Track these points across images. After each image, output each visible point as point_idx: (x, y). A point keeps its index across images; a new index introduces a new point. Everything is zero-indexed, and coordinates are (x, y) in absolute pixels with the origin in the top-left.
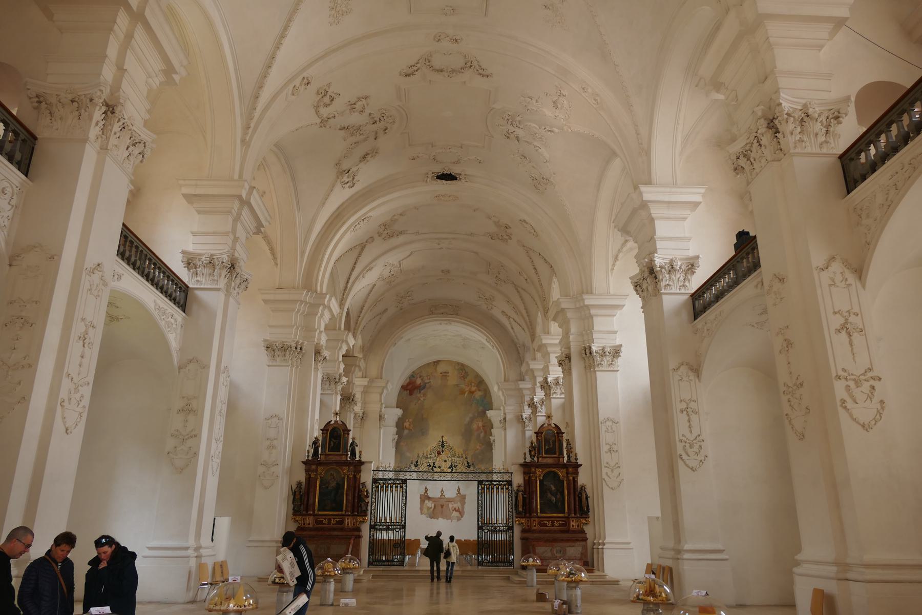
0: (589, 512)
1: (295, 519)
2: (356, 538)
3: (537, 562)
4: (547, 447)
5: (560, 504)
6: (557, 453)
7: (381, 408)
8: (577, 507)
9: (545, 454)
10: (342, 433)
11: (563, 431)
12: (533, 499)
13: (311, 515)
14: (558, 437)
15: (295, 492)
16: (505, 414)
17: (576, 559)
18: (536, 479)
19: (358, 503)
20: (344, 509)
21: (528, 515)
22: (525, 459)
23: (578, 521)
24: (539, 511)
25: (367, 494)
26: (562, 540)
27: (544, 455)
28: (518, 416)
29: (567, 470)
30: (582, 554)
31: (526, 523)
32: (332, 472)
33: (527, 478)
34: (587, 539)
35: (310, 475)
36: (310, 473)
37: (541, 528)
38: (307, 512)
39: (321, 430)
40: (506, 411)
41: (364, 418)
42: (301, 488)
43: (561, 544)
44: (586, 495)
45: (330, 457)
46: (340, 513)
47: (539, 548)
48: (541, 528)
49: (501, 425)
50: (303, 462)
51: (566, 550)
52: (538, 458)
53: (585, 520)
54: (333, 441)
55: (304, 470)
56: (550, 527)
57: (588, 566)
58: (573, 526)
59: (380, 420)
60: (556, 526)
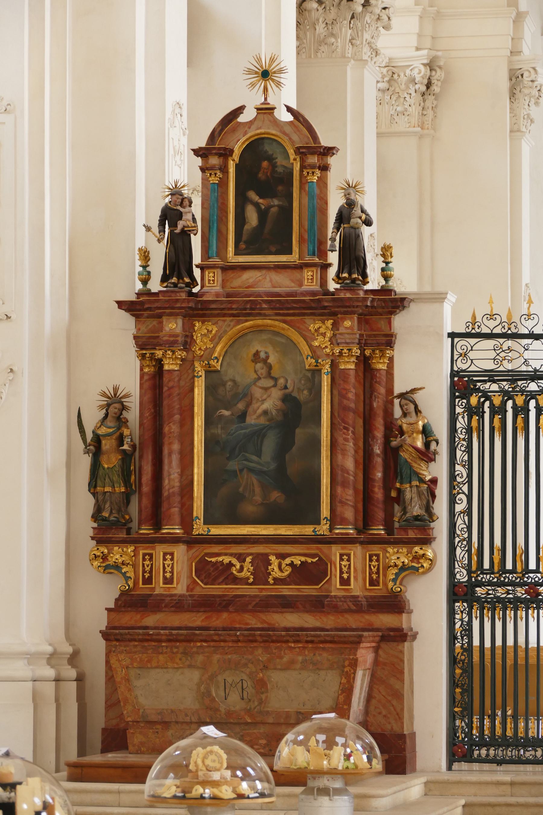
1: (105, 558)
2: (384, 639)
7: (516, 39)
10: (297, 167)
13: (175, 540)
15: (97, 440)
19: (387, 485)
20: (325, 511)
25: (427, 445)
32: (257, 346)
35: (159, 363)
36: (159, 354)
38: (157, 525)
39: (197, 152)
41: (436, 88)
42: (121, 422)
45: (249, 277)
46: (308, 530)
50: (121, 304)
54: (257, 205)
55: (132, 342)
59: (512, 95)
60: (277, 581)
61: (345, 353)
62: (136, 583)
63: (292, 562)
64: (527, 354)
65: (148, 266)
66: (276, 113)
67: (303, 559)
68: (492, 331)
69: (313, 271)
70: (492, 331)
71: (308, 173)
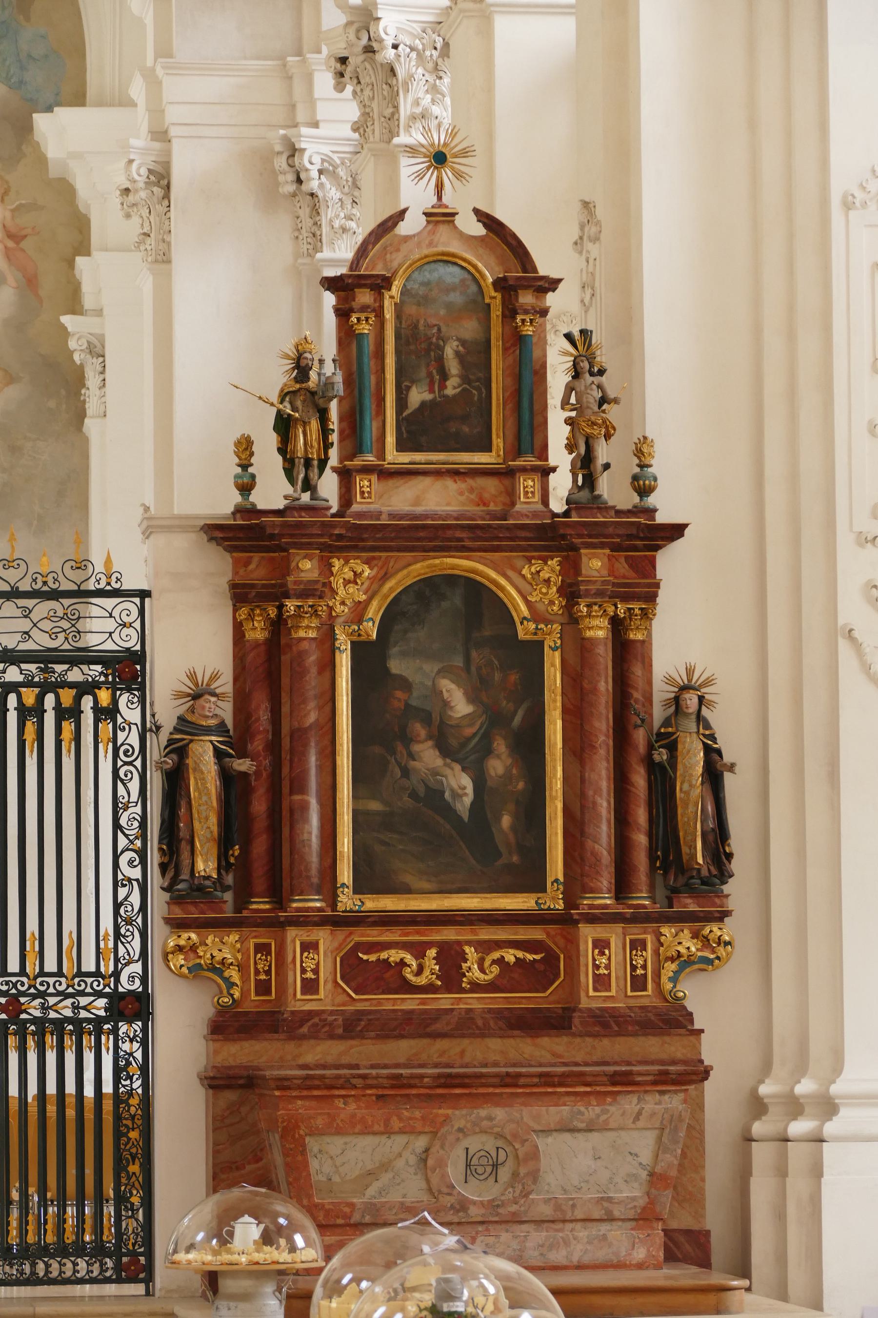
0: (724, 875)
3: (293, 1249)
4: (417, 396)
5: (506, 821)
6: (498, 442)
8: (641, 839)
9: (401, 447)
11: (545, 268)
12: (299, 785)
14: (510, 312)
16: (161, 135)
17: (610, 1219)
18: (333, 637)
21: (260, 905)
22: (246, 487)
23: (638, 945)
24: (345, 874)
26: (509, 1080)
27: (393, 456)
28: (266, 157)
29: (571, 567)
30: (656, 1179)
31: (242, 968)
33: (257, 632)
34: (705, 1074)
37: (366, 1002)
40: (173, 115)
43: (500, 1113)
44: (712, 754)
47: (335, 1144)
48: (366, 1002)
49: (133, 227)
51: (534, 1155)
52: (345, 475)
53: (695, 935)
56: (429, 988)
57: (705, 1263)
58: (602, 982)
60: (476, 987)
61: (636, 615)
62: (244, 994)
63: (503, 957)
64: (26, 625)
65: (251, 465)
66: (458, 220)
67: (520, 954)
68: (79, 586)
69: (533, 480)
70: (79, 586)
71: (359, 319)
